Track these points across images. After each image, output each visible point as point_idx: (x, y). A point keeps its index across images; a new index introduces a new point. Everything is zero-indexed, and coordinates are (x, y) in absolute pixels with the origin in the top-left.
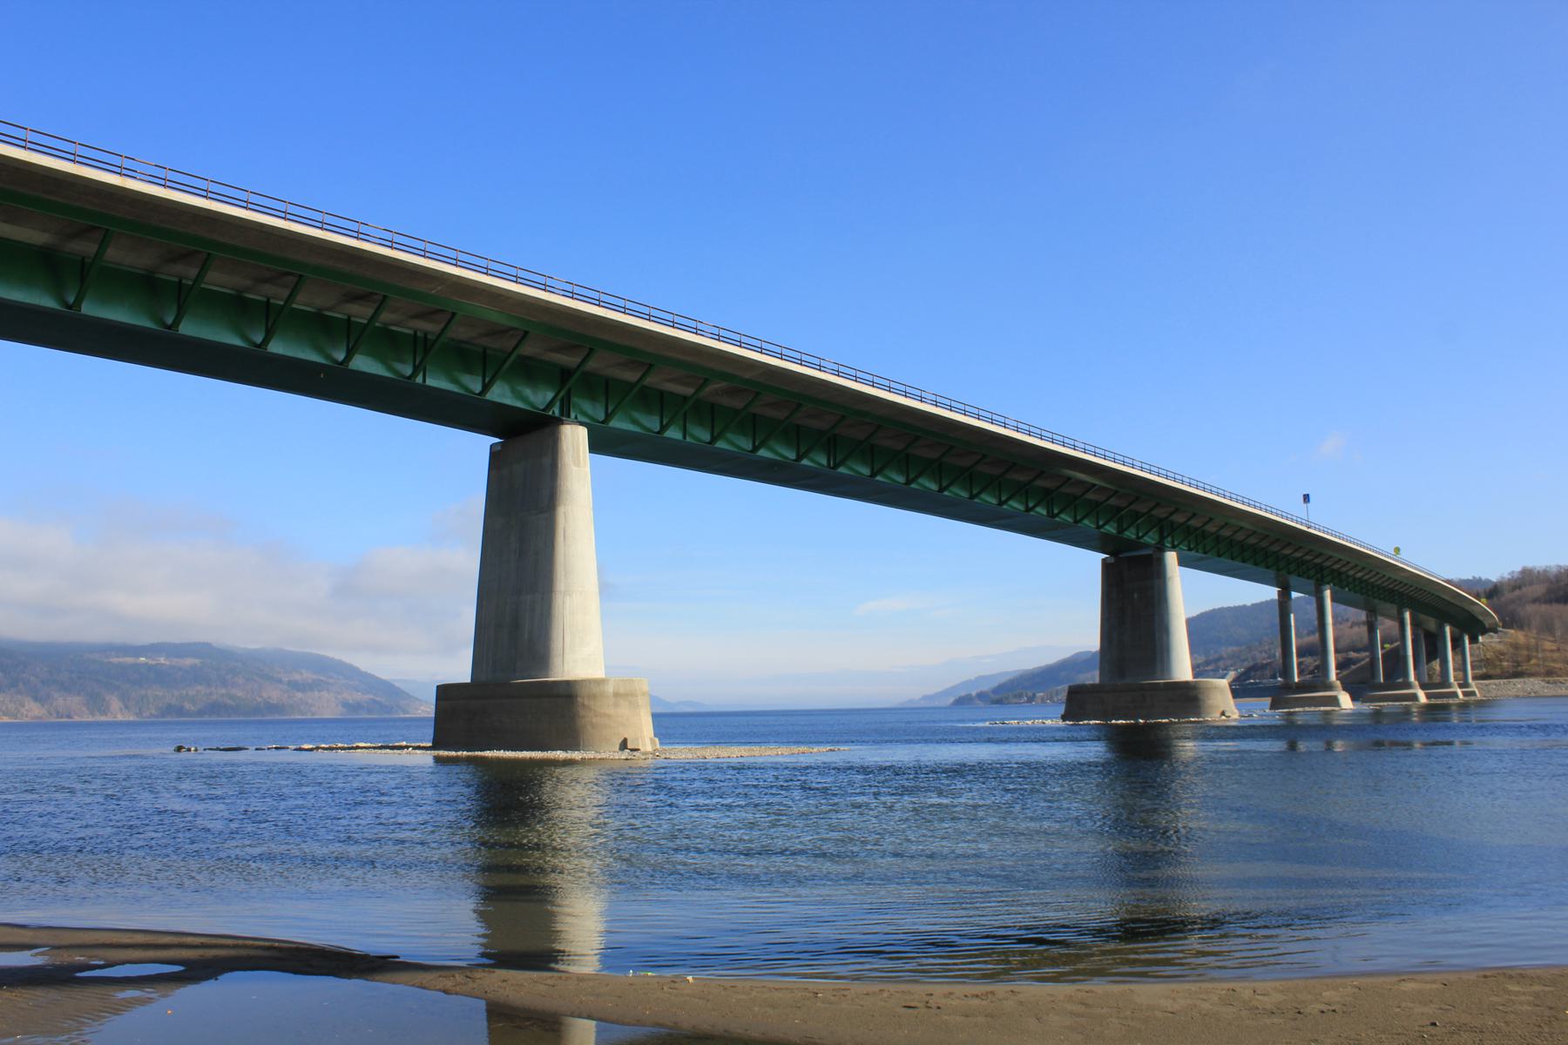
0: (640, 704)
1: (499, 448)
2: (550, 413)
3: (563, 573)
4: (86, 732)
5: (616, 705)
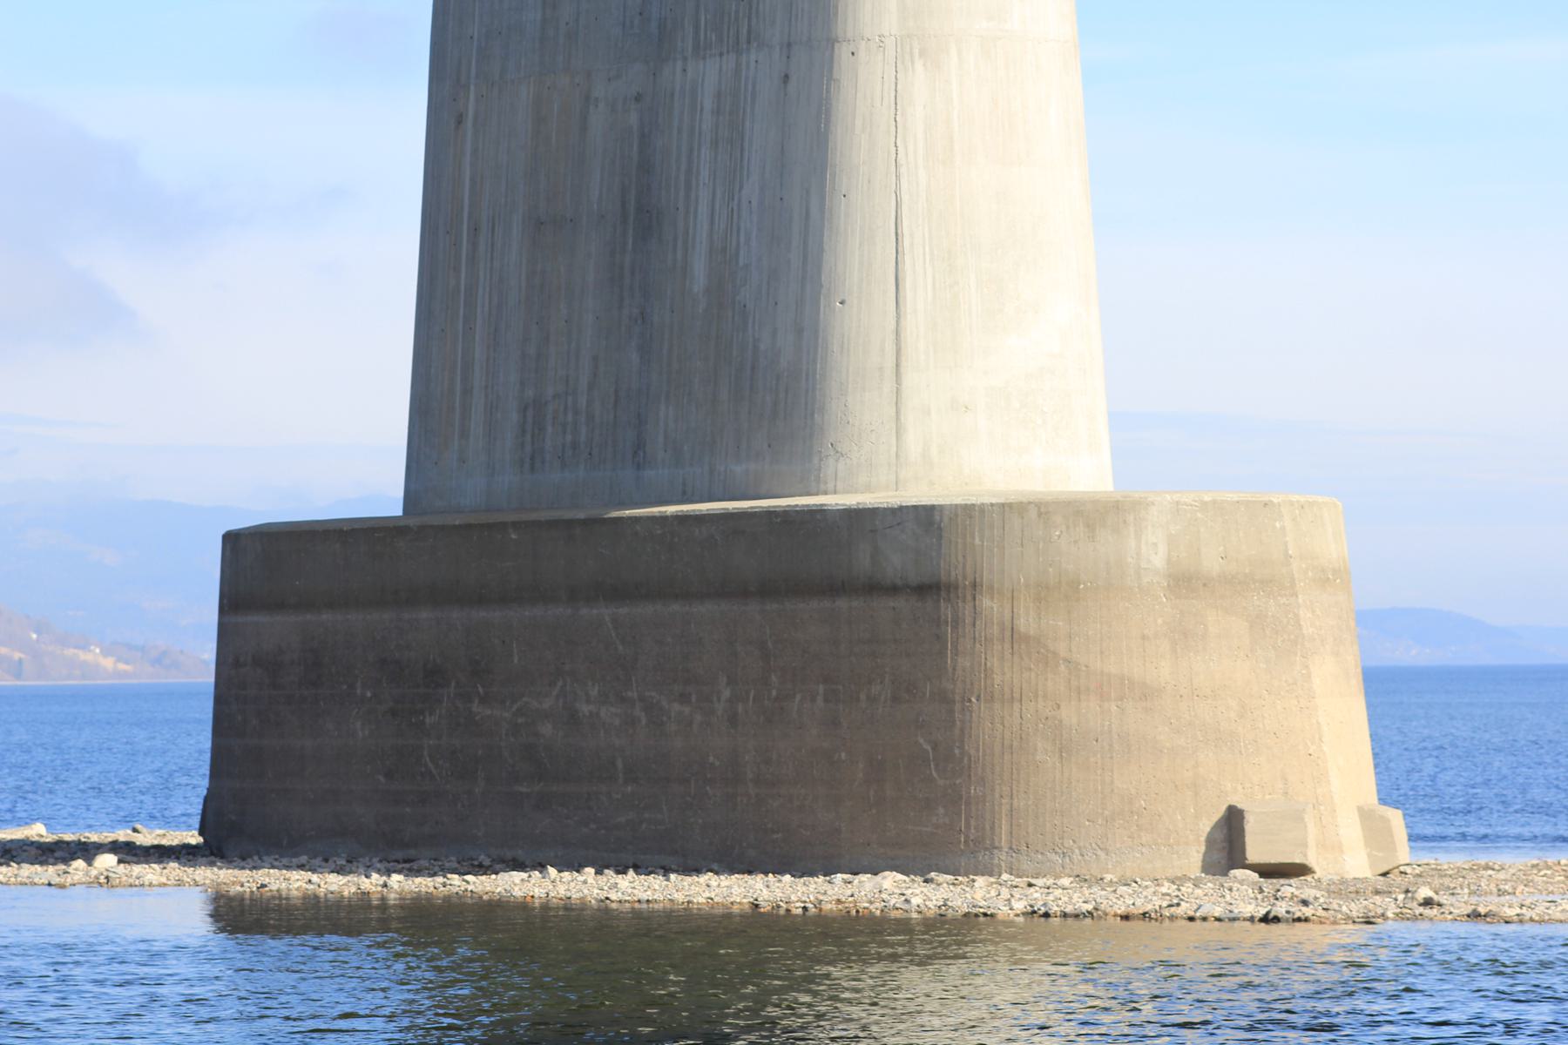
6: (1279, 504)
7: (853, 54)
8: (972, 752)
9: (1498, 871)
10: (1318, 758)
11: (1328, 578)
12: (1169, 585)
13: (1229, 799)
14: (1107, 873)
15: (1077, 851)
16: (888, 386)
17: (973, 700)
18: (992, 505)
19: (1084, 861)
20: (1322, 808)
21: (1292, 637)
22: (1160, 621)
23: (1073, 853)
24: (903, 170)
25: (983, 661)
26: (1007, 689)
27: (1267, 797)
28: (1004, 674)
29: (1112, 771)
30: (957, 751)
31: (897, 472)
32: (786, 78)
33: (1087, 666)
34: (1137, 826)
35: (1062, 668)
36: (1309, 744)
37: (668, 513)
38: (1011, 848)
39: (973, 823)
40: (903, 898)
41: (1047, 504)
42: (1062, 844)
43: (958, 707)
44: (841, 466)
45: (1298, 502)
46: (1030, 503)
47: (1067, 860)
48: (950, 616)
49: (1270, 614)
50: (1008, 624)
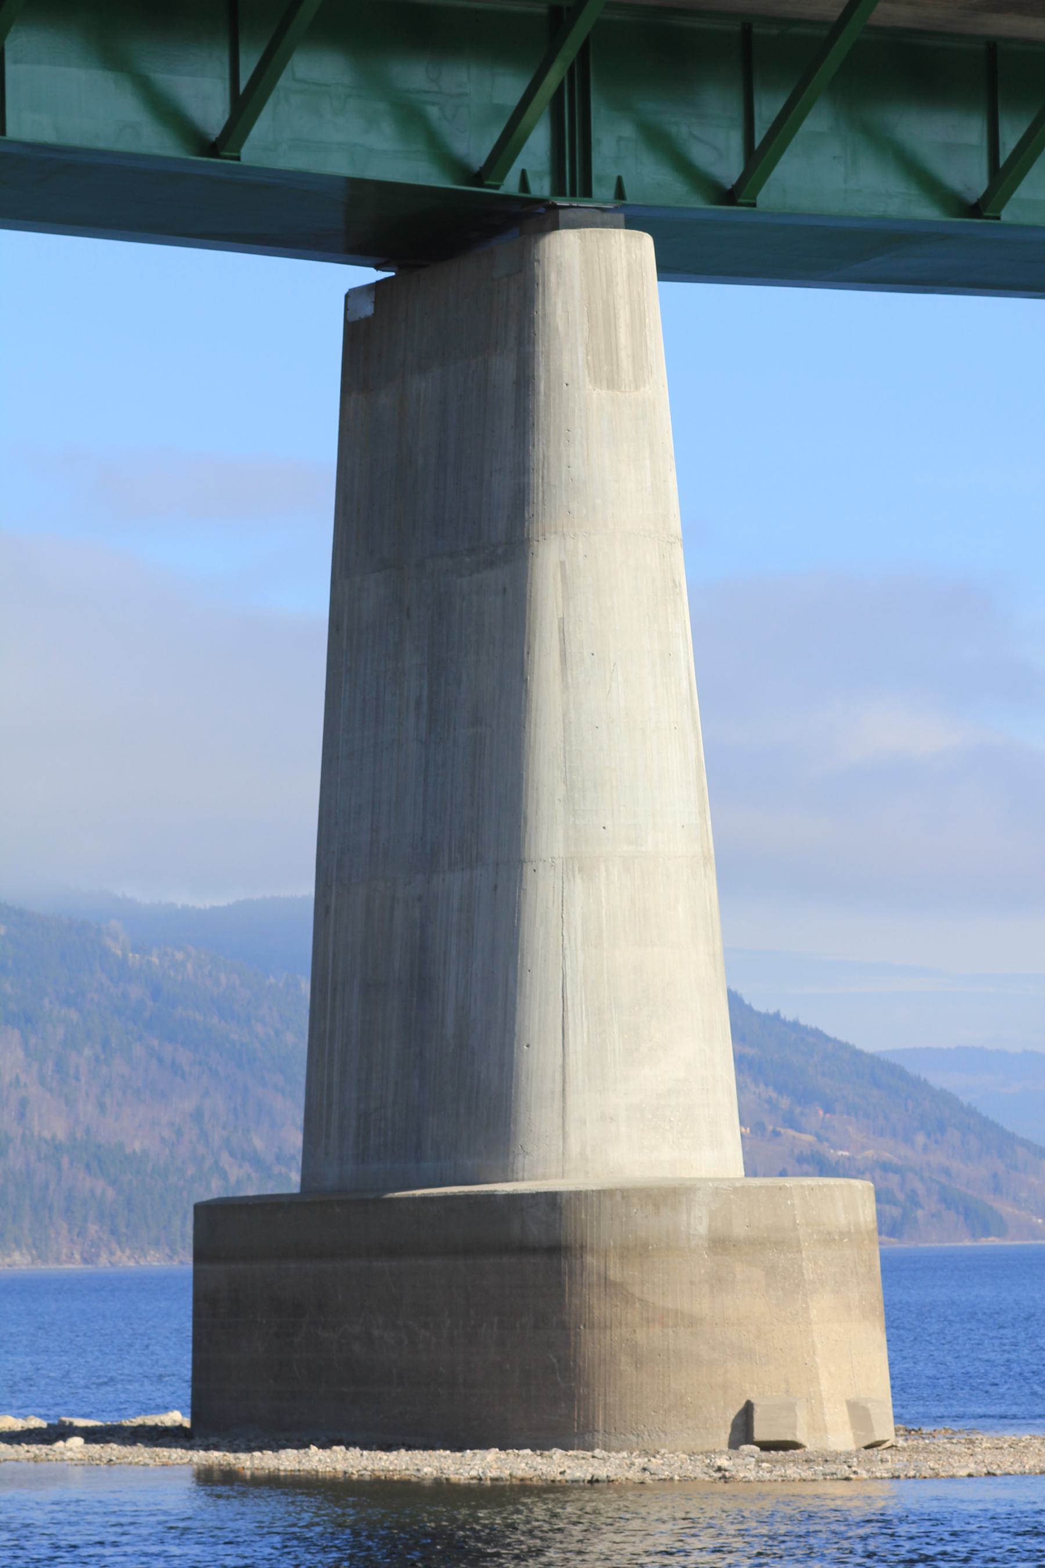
0: (808, 1276)
1: (367, 309)
2: (510, 185)
3: (561, 790)
4: (24, 1267)
5: (719, 1282)
6: (791, 1188)
7: (535, 871)
8: (581, 1364)
9: (956, 1444)
10: (812, 1366)
11: (835, 1239)
12: (709, 1246)
13: (747, 1395)
14: (661, 1448)
15: (646, 1433)
16: (557, 1104)
17: (582, 1327)
18: (593, 1191)
19: (651, 1439)
20: (813, 1401)
21: (796, 1281)
22: (703, 1271)
23: (644, 1434)
24: (567, 952)
25: (587, 1300)
26: (602, 1320)
27: (774, 1394)
28: (600, 1309)
29: (669, 1376)
30: (572, 1364)
31: (563, 1166)
32: (496, 887)
33: (653, 1304)
34: (686, 1415)
35: (637, 1305)
36: (806, 1356)
37: (417, 1195)
38: (605, 1431)
39: (582, 1413)
40: (533, 1469)
41: (628, 1190)
42: (637, 1428)
43: (572, 1333)
44: (527, 1161)
45: (808, 1185)
46: (617, 1189)
47: (640, 1439)
48: (567, 1269)
49: (781, 1265)
50: (603, 1273)
